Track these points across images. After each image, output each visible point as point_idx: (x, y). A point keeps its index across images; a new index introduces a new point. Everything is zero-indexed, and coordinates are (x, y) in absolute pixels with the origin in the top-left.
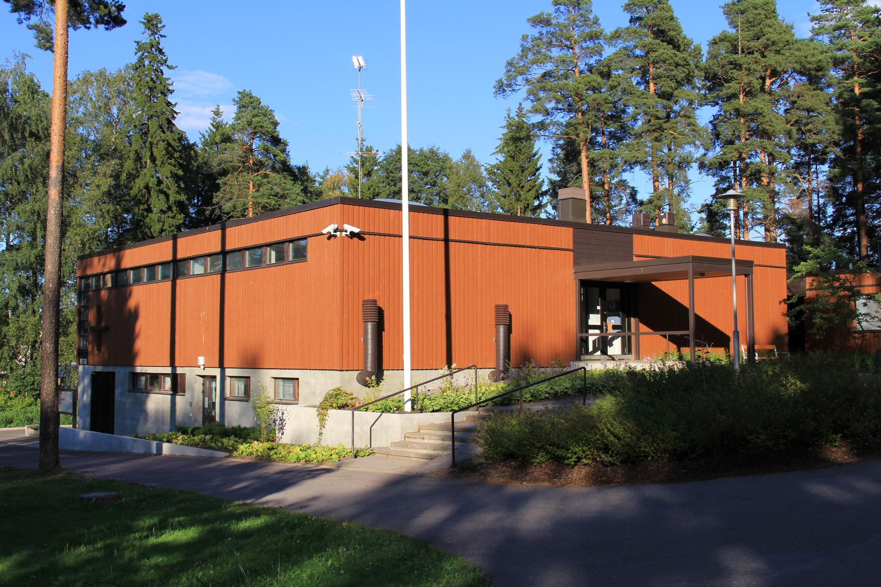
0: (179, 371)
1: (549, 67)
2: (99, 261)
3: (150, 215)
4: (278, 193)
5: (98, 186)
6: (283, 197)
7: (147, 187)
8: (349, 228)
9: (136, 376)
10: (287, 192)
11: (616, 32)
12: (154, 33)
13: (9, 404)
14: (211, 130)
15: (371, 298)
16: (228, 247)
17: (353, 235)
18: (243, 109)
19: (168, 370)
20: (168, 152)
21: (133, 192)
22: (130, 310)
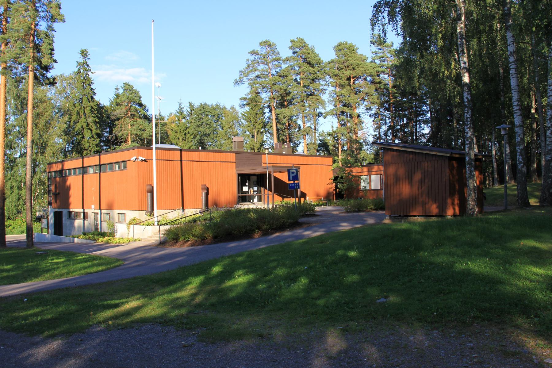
0: (86, 211)
1: (257, 73)
2: (56, 165)
3: (84, 139)
4: (142, 129)
5: (60, 128)
6: (144, 130)
7: (82, 127)
8: (141, 158)
9: (70, 213)
10: (145, 128)
11: (286, 58)
12: (85, 58)
13: (22, 224)
14: (114, 97)
15: (150, 184)
16: (101, 163)
17: (142, 160)
18: (125, 91)
19: (82, 210)
20: (92, 111)
21: (76, 129)
22: (67, 186)
